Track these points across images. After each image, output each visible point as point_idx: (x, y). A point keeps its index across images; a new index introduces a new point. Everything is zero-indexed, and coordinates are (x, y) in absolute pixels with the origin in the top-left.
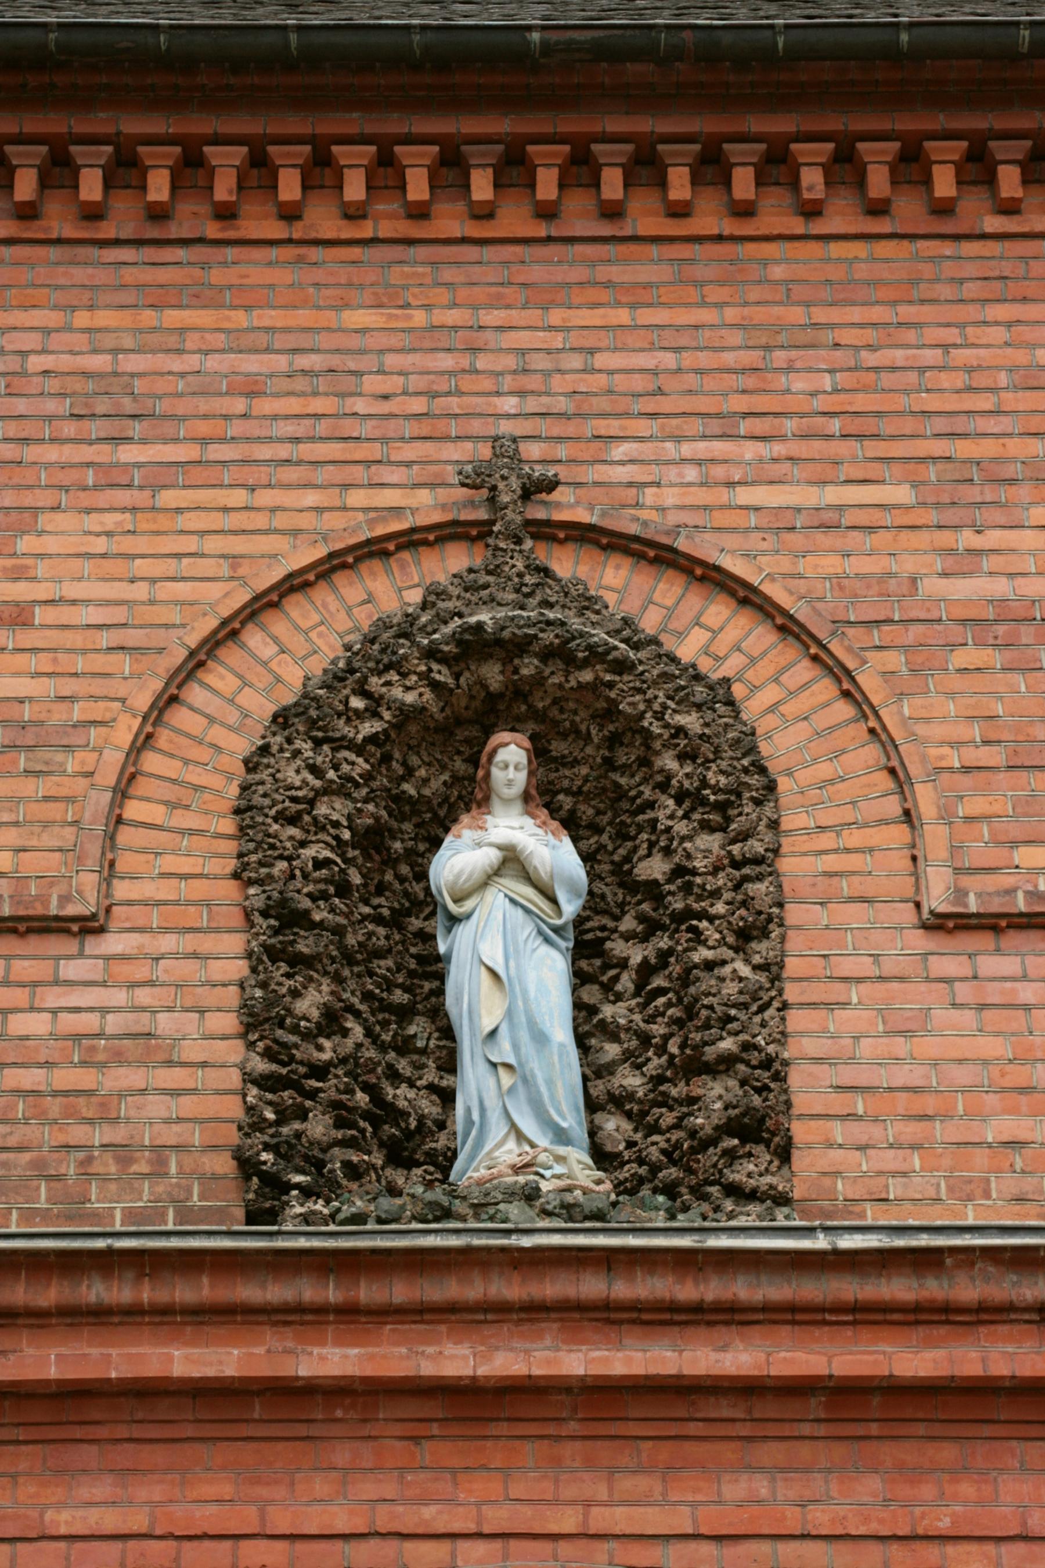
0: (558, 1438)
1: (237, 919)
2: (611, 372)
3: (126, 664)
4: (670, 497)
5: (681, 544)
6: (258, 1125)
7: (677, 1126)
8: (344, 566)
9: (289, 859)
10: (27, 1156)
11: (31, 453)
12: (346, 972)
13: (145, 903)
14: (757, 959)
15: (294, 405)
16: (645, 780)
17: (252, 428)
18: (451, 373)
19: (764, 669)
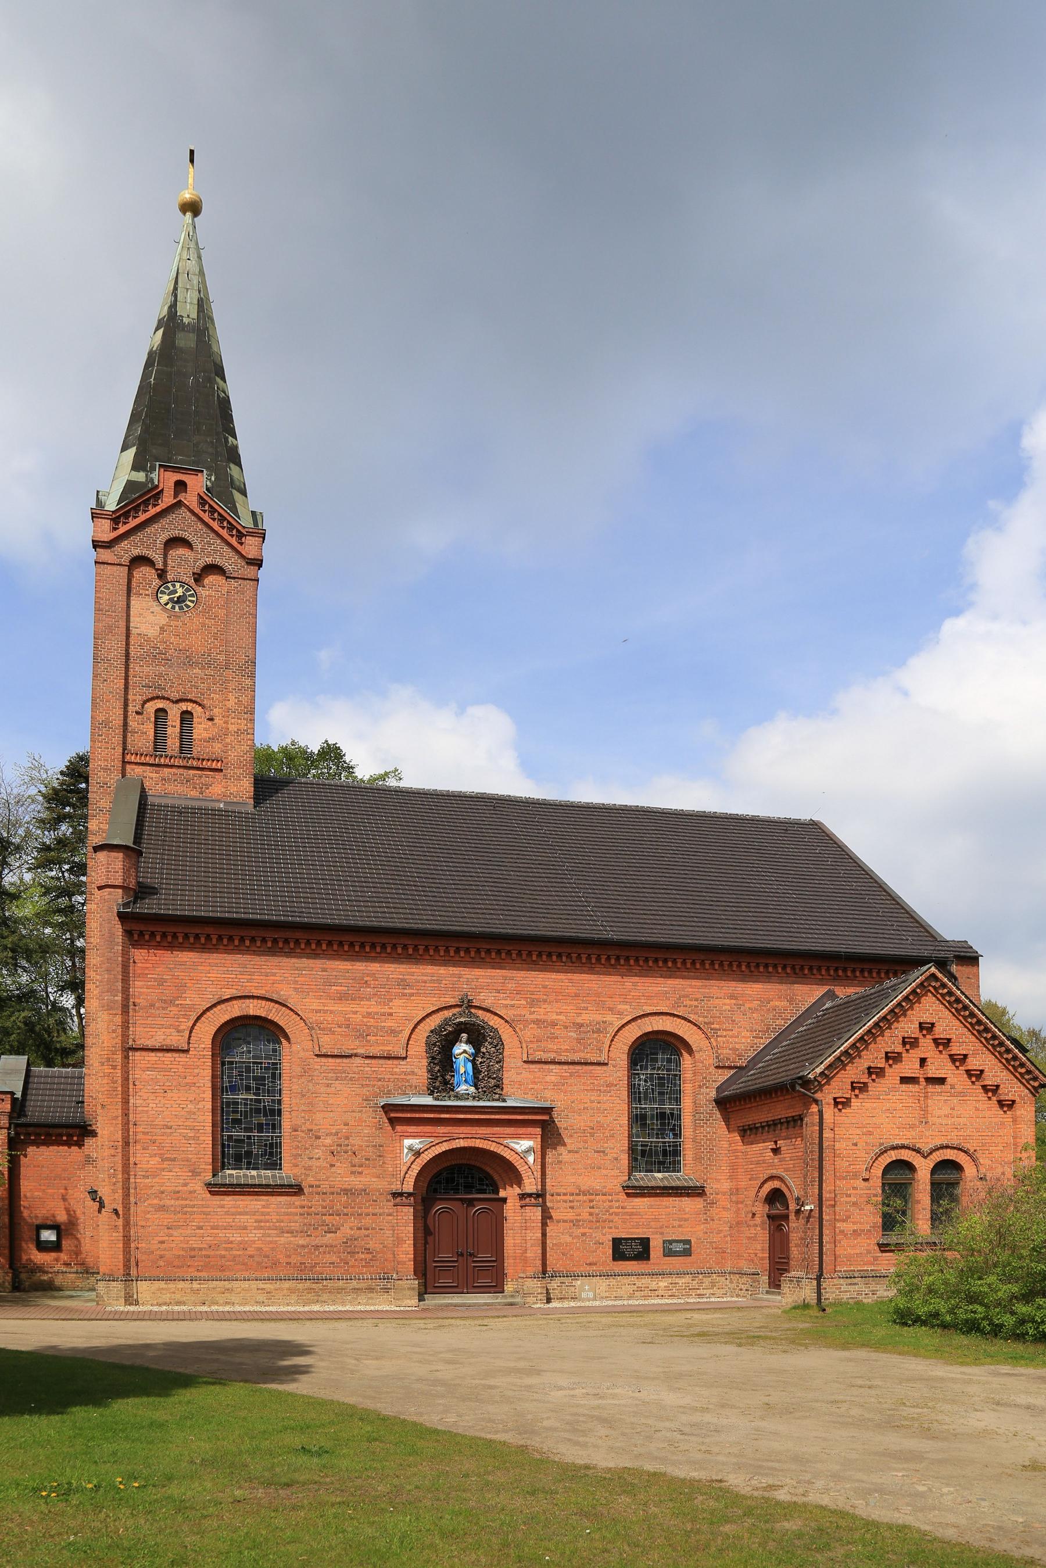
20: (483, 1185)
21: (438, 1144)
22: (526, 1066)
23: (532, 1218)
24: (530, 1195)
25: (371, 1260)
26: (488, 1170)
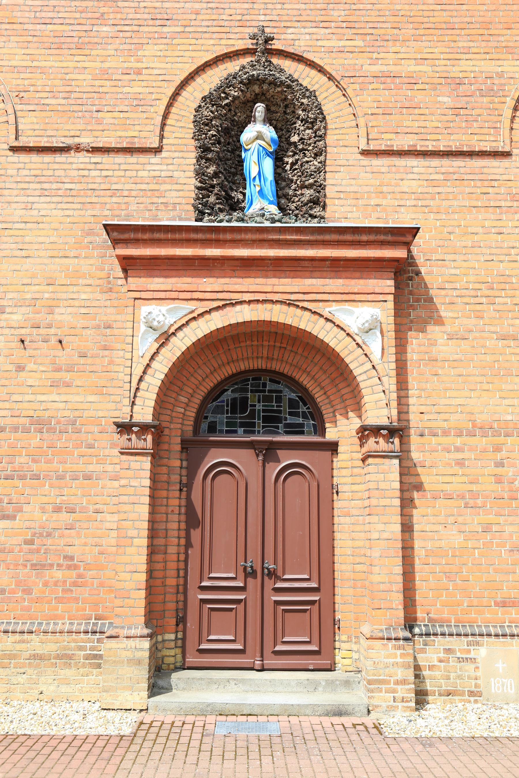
0: (267, 271)
1: (193, 149)
2: (288, 10)
3: (165, 84)
4: (302, 43)
5: (305, 55)
6: (198, 198)
7: (298, 201)
8: (220, 60)
9: (206, 134)
10: (142, 205)
11: (141, 29)
12: (220, 163)
13: (171, 145)
14: (319, 160)
15: (207, 17)
16: (294, 117)
17: (196, 23)
18: (248, 9)
19: (324, 88)
20: (296, 415)
21: (202, 315)
22: (365, 161)
23: (382, 486)
24: (376, 431)
25: (75, 584)
26: (305, 381)
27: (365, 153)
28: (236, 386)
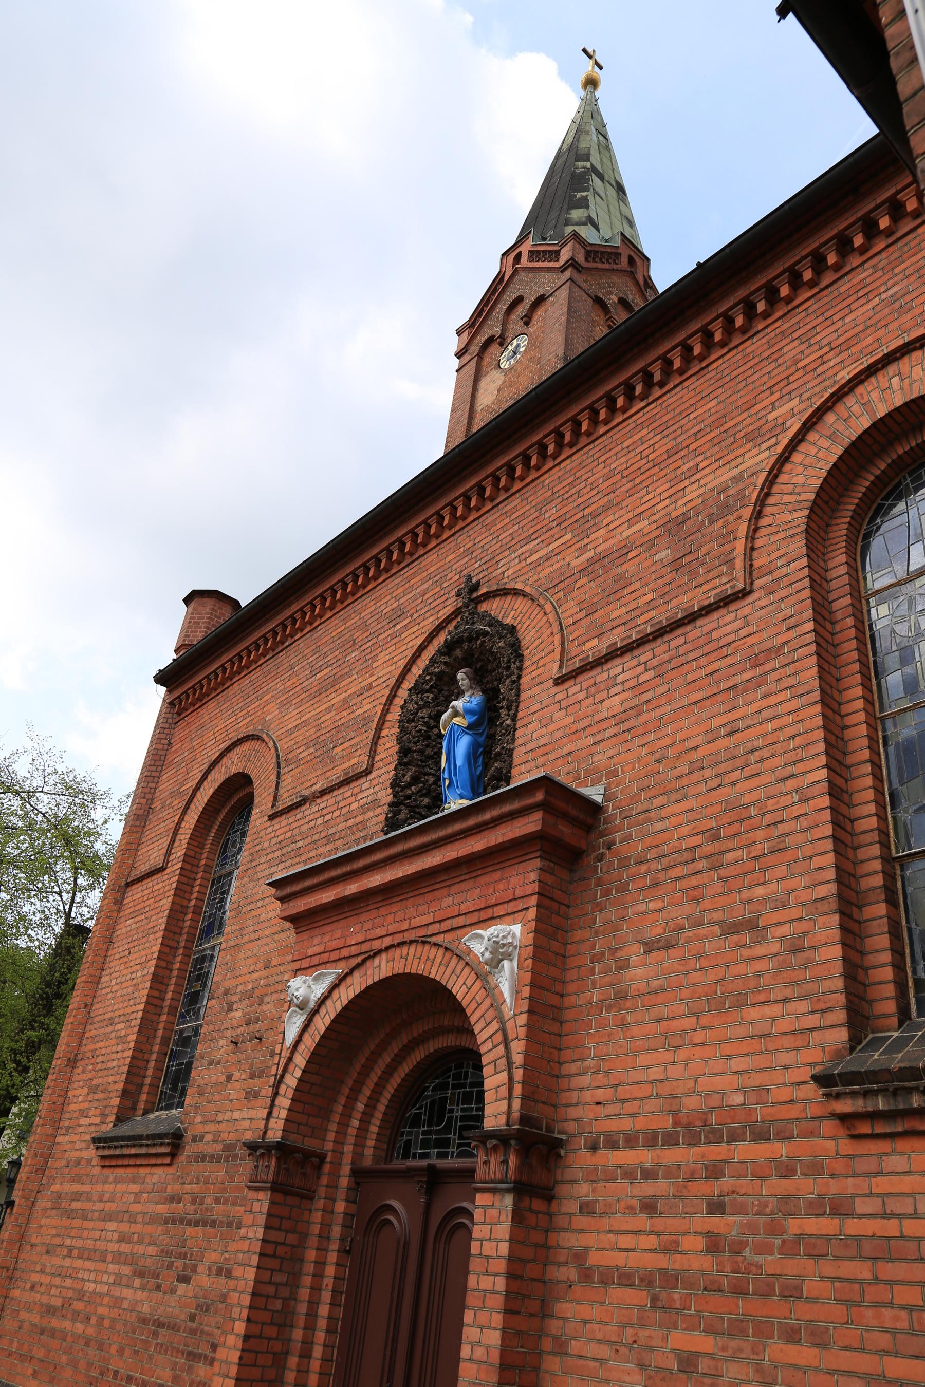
27: (560, 681)
28: (437, 1081)
